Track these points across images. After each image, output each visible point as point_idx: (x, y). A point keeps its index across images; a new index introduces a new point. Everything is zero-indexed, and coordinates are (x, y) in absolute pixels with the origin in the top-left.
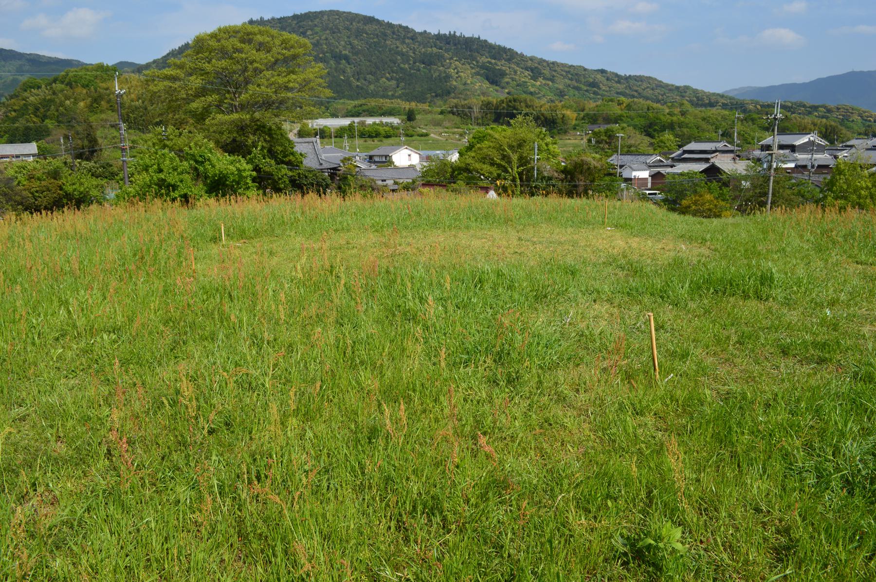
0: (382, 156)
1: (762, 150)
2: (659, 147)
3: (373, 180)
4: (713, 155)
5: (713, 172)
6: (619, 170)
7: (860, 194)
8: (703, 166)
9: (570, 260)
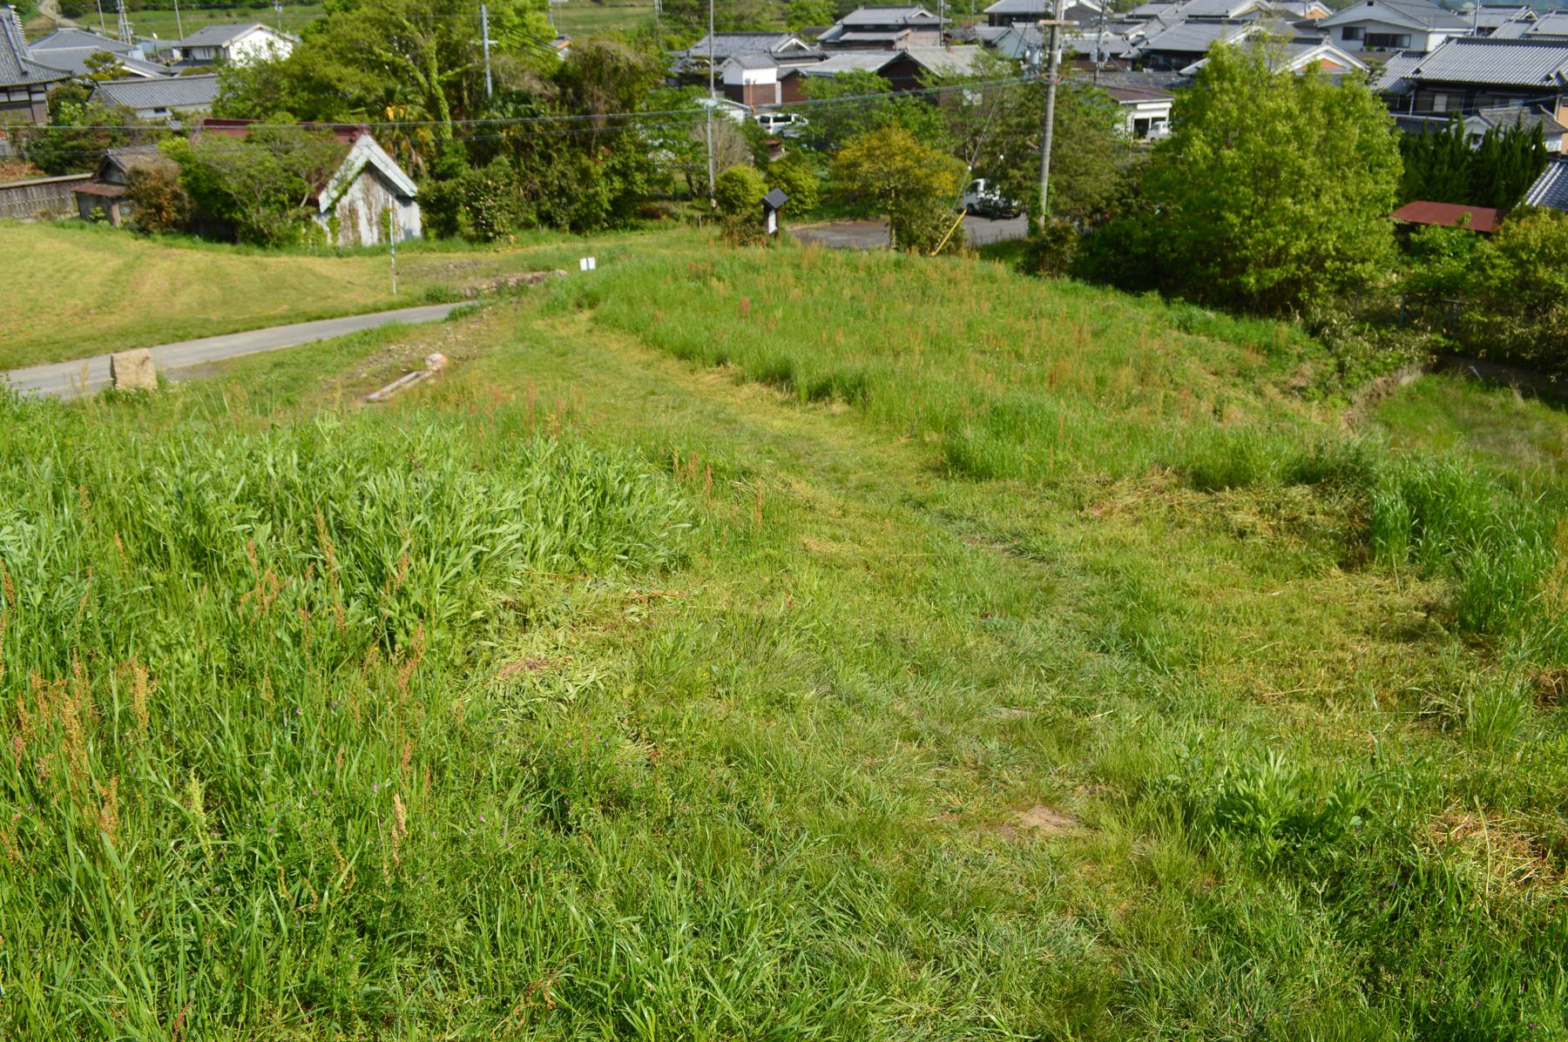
0: (209, 48)
1: (991, 23)
2: (798, 18)
3: (127, 110)
4: (901, 34)
5: (903, 72)
6: (713, 69)
7: (1273, 132)
8: (883, 58)
9: (90, 698)
